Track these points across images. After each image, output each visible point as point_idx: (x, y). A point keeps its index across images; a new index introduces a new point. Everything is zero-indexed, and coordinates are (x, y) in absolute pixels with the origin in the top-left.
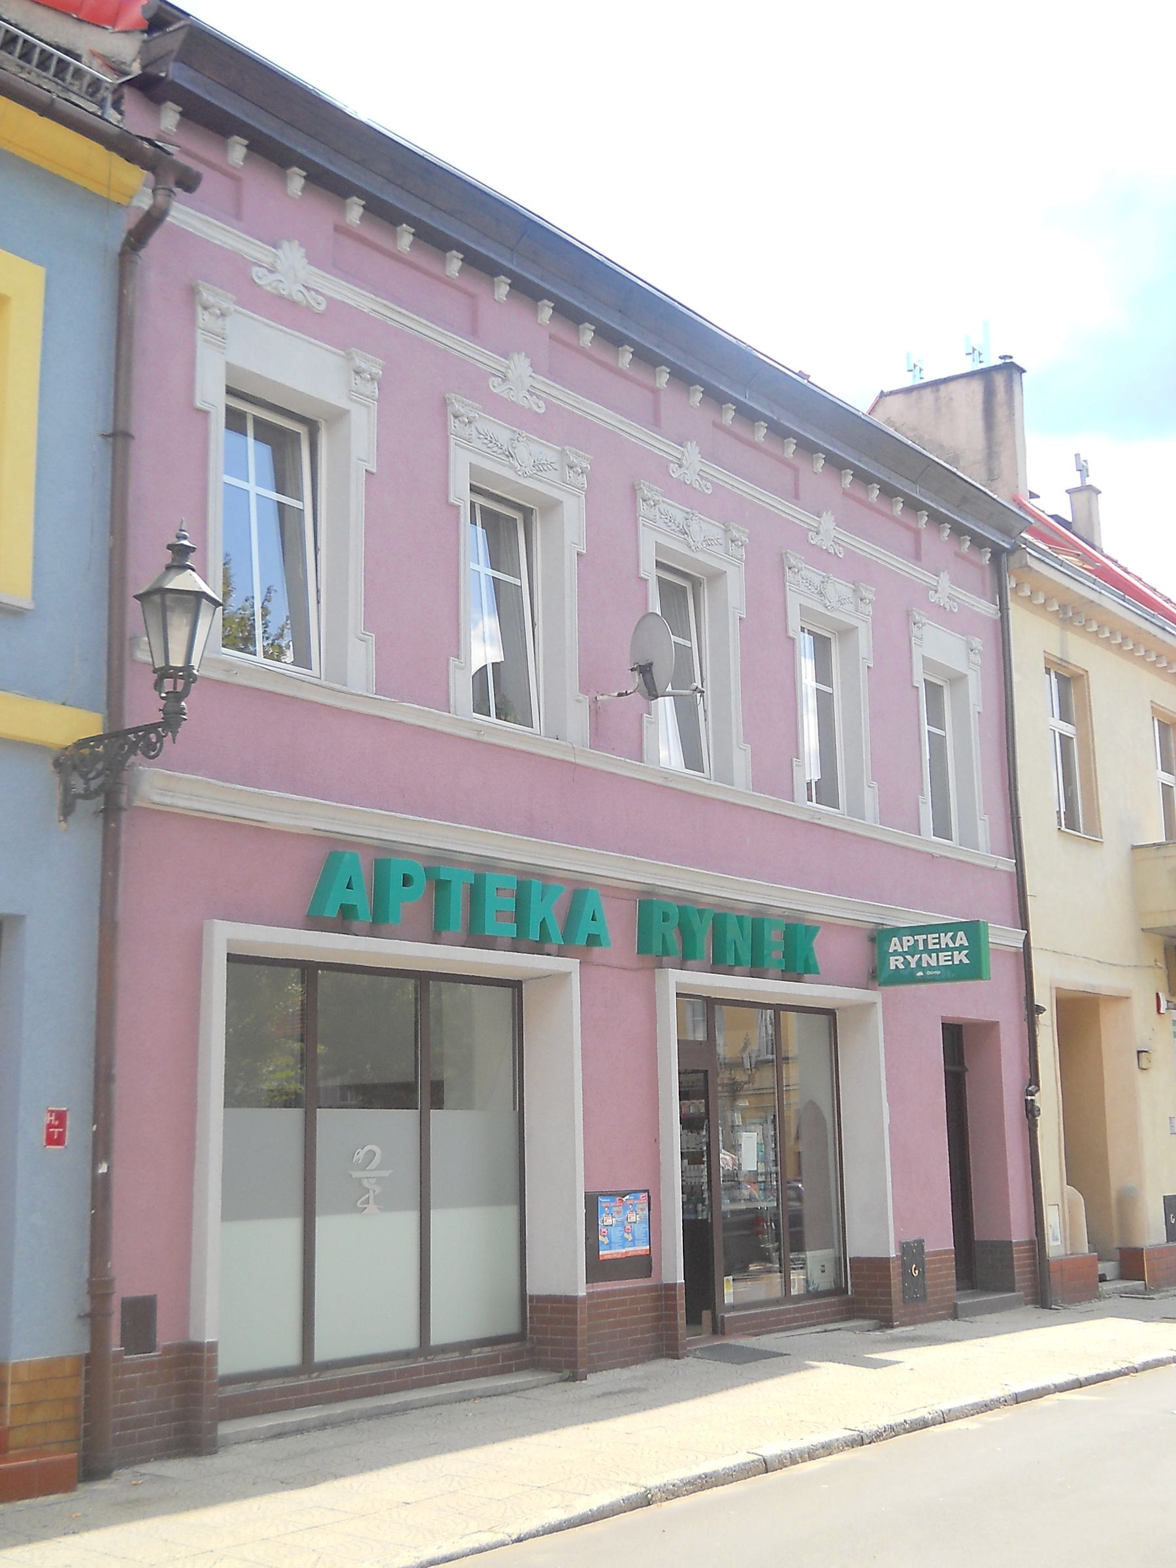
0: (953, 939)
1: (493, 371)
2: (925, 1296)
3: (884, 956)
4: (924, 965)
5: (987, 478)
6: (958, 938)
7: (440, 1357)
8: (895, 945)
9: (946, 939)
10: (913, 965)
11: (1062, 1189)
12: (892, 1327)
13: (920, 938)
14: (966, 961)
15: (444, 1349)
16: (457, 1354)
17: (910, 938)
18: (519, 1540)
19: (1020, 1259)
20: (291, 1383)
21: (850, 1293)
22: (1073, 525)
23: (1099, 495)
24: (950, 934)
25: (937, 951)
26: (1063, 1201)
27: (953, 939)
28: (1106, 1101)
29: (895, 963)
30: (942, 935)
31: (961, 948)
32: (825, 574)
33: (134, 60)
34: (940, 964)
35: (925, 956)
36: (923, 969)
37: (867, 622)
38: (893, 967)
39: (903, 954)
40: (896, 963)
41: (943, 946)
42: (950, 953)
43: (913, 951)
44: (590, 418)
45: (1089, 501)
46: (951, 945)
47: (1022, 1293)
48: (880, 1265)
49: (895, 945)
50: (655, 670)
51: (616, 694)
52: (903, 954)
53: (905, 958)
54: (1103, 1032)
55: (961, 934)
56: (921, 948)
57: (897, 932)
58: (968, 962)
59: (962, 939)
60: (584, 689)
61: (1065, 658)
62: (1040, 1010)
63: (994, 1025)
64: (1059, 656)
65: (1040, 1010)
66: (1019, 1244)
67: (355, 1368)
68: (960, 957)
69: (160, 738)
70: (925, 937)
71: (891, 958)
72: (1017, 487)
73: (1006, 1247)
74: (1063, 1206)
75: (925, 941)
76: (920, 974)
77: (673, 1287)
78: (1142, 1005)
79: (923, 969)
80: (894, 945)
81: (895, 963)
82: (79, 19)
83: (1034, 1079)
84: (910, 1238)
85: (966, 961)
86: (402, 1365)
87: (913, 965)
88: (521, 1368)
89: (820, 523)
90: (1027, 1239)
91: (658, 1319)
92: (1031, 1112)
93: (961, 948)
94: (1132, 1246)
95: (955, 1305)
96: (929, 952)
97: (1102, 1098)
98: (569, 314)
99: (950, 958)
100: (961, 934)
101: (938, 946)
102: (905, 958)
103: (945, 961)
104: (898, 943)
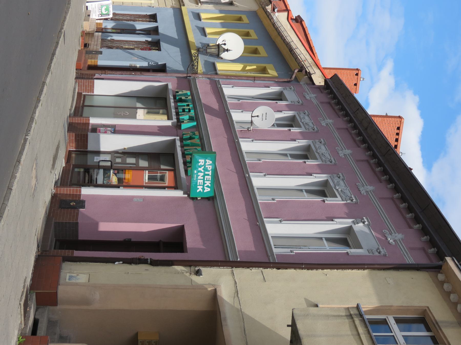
31: (203, 189)
36: (197, 173)
85: (198, 191)
93: (203, 189)
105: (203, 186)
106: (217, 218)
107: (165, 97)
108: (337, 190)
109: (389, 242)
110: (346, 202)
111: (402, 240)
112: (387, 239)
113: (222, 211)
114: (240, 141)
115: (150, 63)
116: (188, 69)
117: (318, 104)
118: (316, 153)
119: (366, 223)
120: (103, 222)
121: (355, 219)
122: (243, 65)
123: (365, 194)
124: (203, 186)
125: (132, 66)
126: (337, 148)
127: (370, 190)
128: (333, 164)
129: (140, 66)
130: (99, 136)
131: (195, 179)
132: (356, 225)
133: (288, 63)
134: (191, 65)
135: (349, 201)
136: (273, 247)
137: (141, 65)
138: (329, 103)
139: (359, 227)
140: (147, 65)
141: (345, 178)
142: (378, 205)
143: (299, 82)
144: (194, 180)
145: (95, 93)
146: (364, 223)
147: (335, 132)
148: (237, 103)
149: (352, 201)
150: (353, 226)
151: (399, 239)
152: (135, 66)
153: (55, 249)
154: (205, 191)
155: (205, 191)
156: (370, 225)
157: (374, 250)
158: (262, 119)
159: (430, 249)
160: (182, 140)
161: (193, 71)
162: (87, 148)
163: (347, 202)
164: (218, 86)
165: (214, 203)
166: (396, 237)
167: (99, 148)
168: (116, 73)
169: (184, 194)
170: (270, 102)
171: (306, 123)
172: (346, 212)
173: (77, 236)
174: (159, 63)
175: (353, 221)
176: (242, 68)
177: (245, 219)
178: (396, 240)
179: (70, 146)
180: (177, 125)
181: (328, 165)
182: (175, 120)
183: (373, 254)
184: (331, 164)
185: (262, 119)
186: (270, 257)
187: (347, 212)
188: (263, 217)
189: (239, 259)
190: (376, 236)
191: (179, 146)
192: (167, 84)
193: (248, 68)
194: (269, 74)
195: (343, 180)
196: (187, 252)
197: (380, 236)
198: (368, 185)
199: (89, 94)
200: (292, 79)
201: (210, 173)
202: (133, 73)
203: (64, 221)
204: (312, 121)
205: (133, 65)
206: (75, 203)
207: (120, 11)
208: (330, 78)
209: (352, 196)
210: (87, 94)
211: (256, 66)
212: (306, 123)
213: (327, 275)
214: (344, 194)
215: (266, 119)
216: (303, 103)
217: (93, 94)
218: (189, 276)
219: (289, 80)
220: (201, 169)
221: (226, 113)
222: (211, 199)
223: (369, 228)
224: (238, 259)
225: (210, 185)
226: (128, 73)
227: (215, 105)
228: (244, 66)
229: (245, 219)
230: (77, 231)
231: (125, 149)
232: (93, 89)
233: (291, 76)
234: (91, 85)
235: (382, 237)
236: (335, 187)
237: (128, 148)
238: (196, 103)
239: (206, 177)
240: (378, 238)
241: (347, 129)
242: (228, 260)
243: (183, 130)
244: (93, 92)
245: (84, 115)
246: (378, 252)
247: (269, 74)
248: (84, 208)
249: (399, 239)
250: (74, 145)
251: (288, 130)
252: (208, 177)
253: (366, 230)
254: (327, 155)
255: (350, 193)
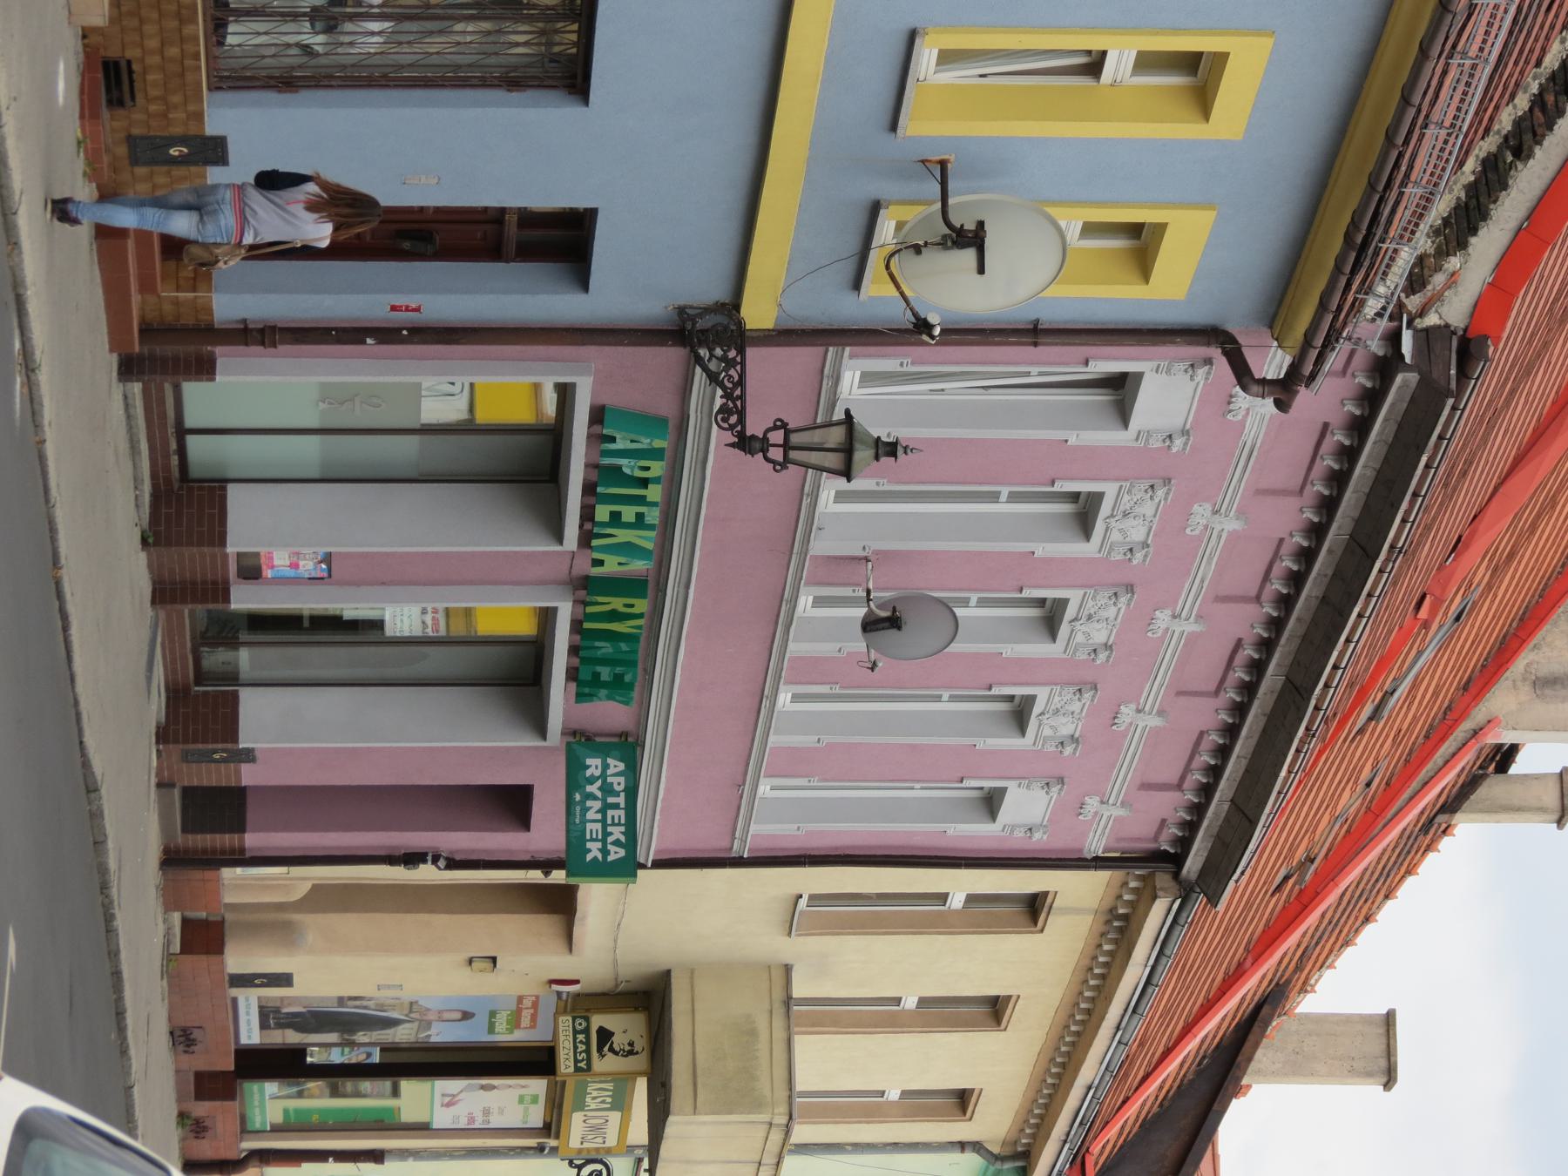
0: (617, 843)
2: (187, 762)
3: (603, 751)
4: (589, 803)
5: (1539, 674)
6: (618, 849)
8: (615, 766)
9: (617, 833)
10: (589, 788)
11: (309, 879)
12: (158, 742)
13: (621, 800)
14: (589, 857)
17: (622, 787)
19: (226, 840)
20: (171, 413)
21: (197, 688)
22: (1500, 777)
23: (1555, 825)
24: (623, 839)
25: (603, 821)
26: (291, 879)
27: (617, 843)
28: (426, 915)
29: (594, 765)
30: (623, 829)
31: (605, 851)
32: (1084, 714)
33: (1441, 318)
34: (588, 824)
35: (597, 805)
37: (1034, 744)
38: (589, 761)
39: (604, 776)
40: (594, 767)
42: (600, 837)
43: (607, 790)
45: (1542, 810)
46: (610, 839)
47: (180, 840)
48: (230, 730)
49: (615, 766)
50: (894, 631)
51: (871, 586)
52: (604, 776)
53: (598, 778)
54: (516, 916)
55: (622, 853)
56: (611, 800)
57: (633, 771)
58: (588, 860)
59: (617, 853)
60: (877, 552)
61: (1052, 911)
62: (547, 874)
63: (526, 825)
64: (1054, 905)
65: (547, 874)
66: (242, 840)
68: (594, 850)
69: (732, 428)
70: (622, 806)
71: (600, 760)
72: (1514, 729)
73: (240, 828)
74: (286, 879)
75: (616, 806)
76: (578, 797)
77: (227, 599)
78: (562, 965)
79: (583, 802)
80: (616, 766)
81: (594, 765)
82: (1520, 229)
83: (453, 864)
84: (257, 753)
85: (589, 857)
86: (171, 413)
87: (589, 788)
88: (155, 486)
89: (1150, 714)
90: (246, 846)
91: (194, 583)
92: (412, 859)
93: (605, 851)
94: (226, 939)
95: (172, 785)
96: (603, 811)
97: (432, 911)
99: (594, 836)
100: (622, 853)
101: (609, 822)
102: (598, 778)
103: (591, 831)
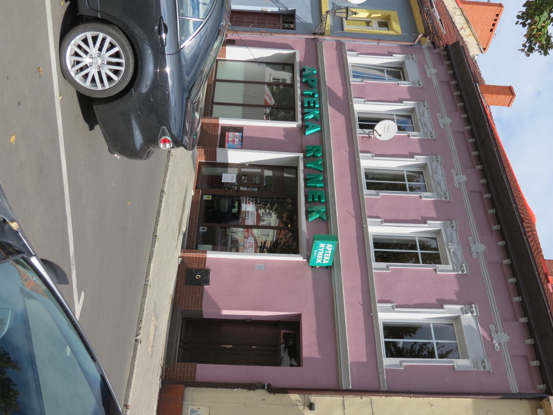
1: (496, 324)
7: (211, 106)
10: (320, 250)
15: (212, 108)
16: (210, 110)
18: (186, 190)
31: (322, 261)
36: (317, 252)
38: (320, 245)
41: (324, 257)
44: (471, 228)
46: (322, 253)
67: (339, 378)
85: (317, 262)
93: (322, 261)
96: (324, 254)
98: (454, 77)
104: (330, 246)
105: (323, 259)
106: (336, 347)
107: (293, 63)
108: (449, 250)
109: (494, 345)
110: (457, 273)
111: (450, 124)
112: (492, 340)
113: (342, 354)
114: (354, 102)
115: (281, 9)
116: (316, 29)
117: (437, 87)
118: (419, 121)
119: (475, 314)
120: (224, 309)
121: (463, 306)
122: (368, 12)
123: (443, 127)
124: (323, 259)
125: (263, 11)
126: (457, 187)
127: (481, 250)
128: (448, 200)
129: (270, 11)
130: (227, 151)
131: (315, 255)
132: (464, 315)
133: (413, 14)
134: (319, 25)
135: (460, 272)
136: (351, 74)
137: (272, 10)
138: (448, 83)
139: (468, 319)
140: (278, 10)
141: (458, 229)
142: (489, 285)
143: (421, 46)
144: (314, 256)
145: (227, 58)
146: (472, 312)
147: (452, 142)
148: (361, 84)
149: (463, 271)
150: (462, 316)
151: (504, 342)
152: (266, 11)
153: (178, 362)
154: (323, 263)
155: (323, 263)
156: (442, 164)
157: (479, 362)
158: (384, 131)
159: (455, 92)
160: (305, 157)
161: (321, 30)
162: (216, 161)
163: (458, 273)
164: (343, 56)
165: (331, 273)
166: (446, 120)
167: (228, 161)
168: (247, 34)
169: (303, 259)
170: (392, 83)
171: (425, 124)
172: (456, 290)
173: (203, 316)
174: (289, 9)
175: (462, 308)
176: (367, 15)
177: (360, 303)
178: (501, 343)
179: (200, 158)
180: (302, 125)
181: (429, 139)
182: (300, 122)
183: (478, 369)
184: (445, 200)
185: (384, 131)
186: (380, 375)
187: (457, 290)
188: (346, 49)
189: (351, 387)
190: (482, 336)
191: (302, 170)
192: (295, 53)
193: (373, 16)
194: (392, 30)
195: (440, 164)
196: (302, 366)
197: (485, 335)
198: (479, 242)
199: (222, 59)
200: (415, 43)
201: (330, 252)
202: (264, 34)
203: (189, 309)
204: (431, 120)
205: (264, 10)
206: (200, 275)
207: (235, 309)
208: (452, 45)
209: (464, 264)
210: (220, 59)
211: (382, 14)
212: (425, 124)
213: (432, 406)
214: (456, 257)
215: (388, 132)
216: (423, 86)
217: (224, 59)
218: (303, 410)
219: (412, 43)
220: (322, 250)
221: (349, 105)
222: (328, 268)
223: (476, 320)
224: (350, 387)
225: (329, 259)
226: (258, 34)
227: (339, 92)
228: (369, 14)
229: (360, 303)
230: (202, 314)
231: (251, 162)
232: (225, 55)
233: (414, 40)
234: (223, 52)
235: (488, 337)
236: (448, 245)
237: (254, 162)
238: (329, 204)
239: (325, 254)
240: (484, 338)
241: (463, 132)
242: (340, 388)
243: (307, 135)
244: (225, 57)
245: (214, 115)
246: (483, 366)
247: (392, 30)
248: (209, 285)
249: (463, 182)
250: (204, 157)
251: (407, 135)
252: (327, 255)
253: (473, 323)
254: (442, 184)
255: (462, 257)
